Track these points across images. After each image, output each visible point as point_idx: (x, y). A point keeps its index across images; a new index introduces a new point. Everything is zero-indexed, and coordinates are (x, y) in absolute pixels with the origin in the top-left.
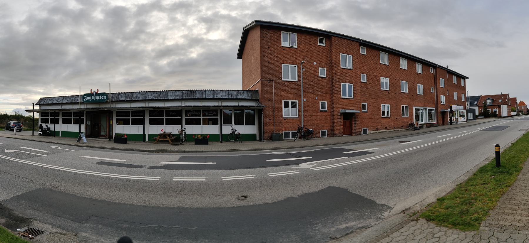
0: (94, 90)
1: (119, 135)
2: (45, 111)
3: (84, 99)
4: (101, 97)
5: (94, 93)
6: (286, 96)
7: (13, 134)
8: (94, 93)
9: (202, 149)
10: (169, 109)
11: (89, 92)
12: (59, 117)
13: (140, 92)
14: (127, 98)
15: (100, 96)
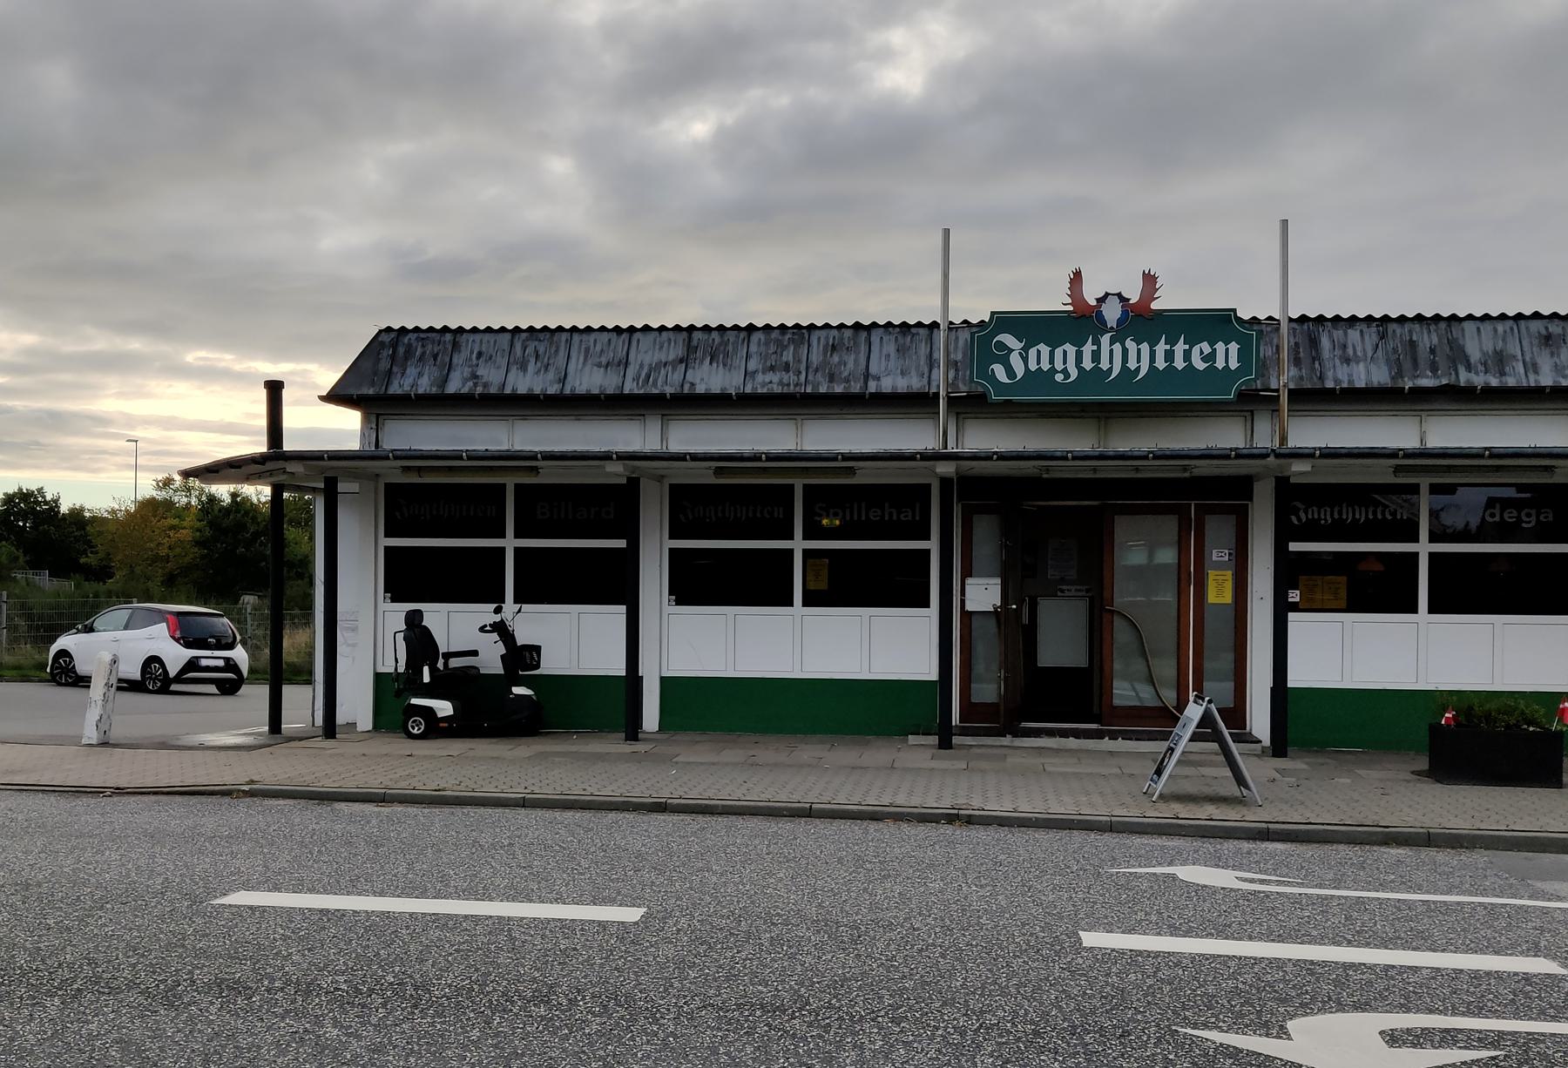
1: (1492, 706)
4: (1180, 347)
5: (1112, 313)
7: (75, 741)
8: (1112, 313)
10: (851, 471)
11: (1056, 300)
14: (1407, 365)
15: (1172, 342)
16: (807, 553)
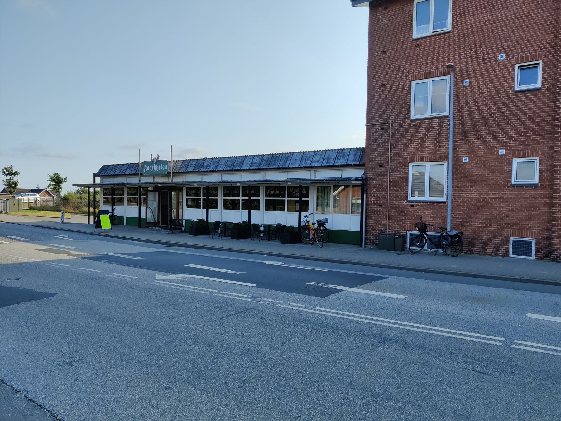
0: (155, 156)
4: (161, 166)
5: (155, 161)
6: (417, 155)
8: (155, 161)
11: (149, 160)
12: (259, 197)
16: (242, 200)
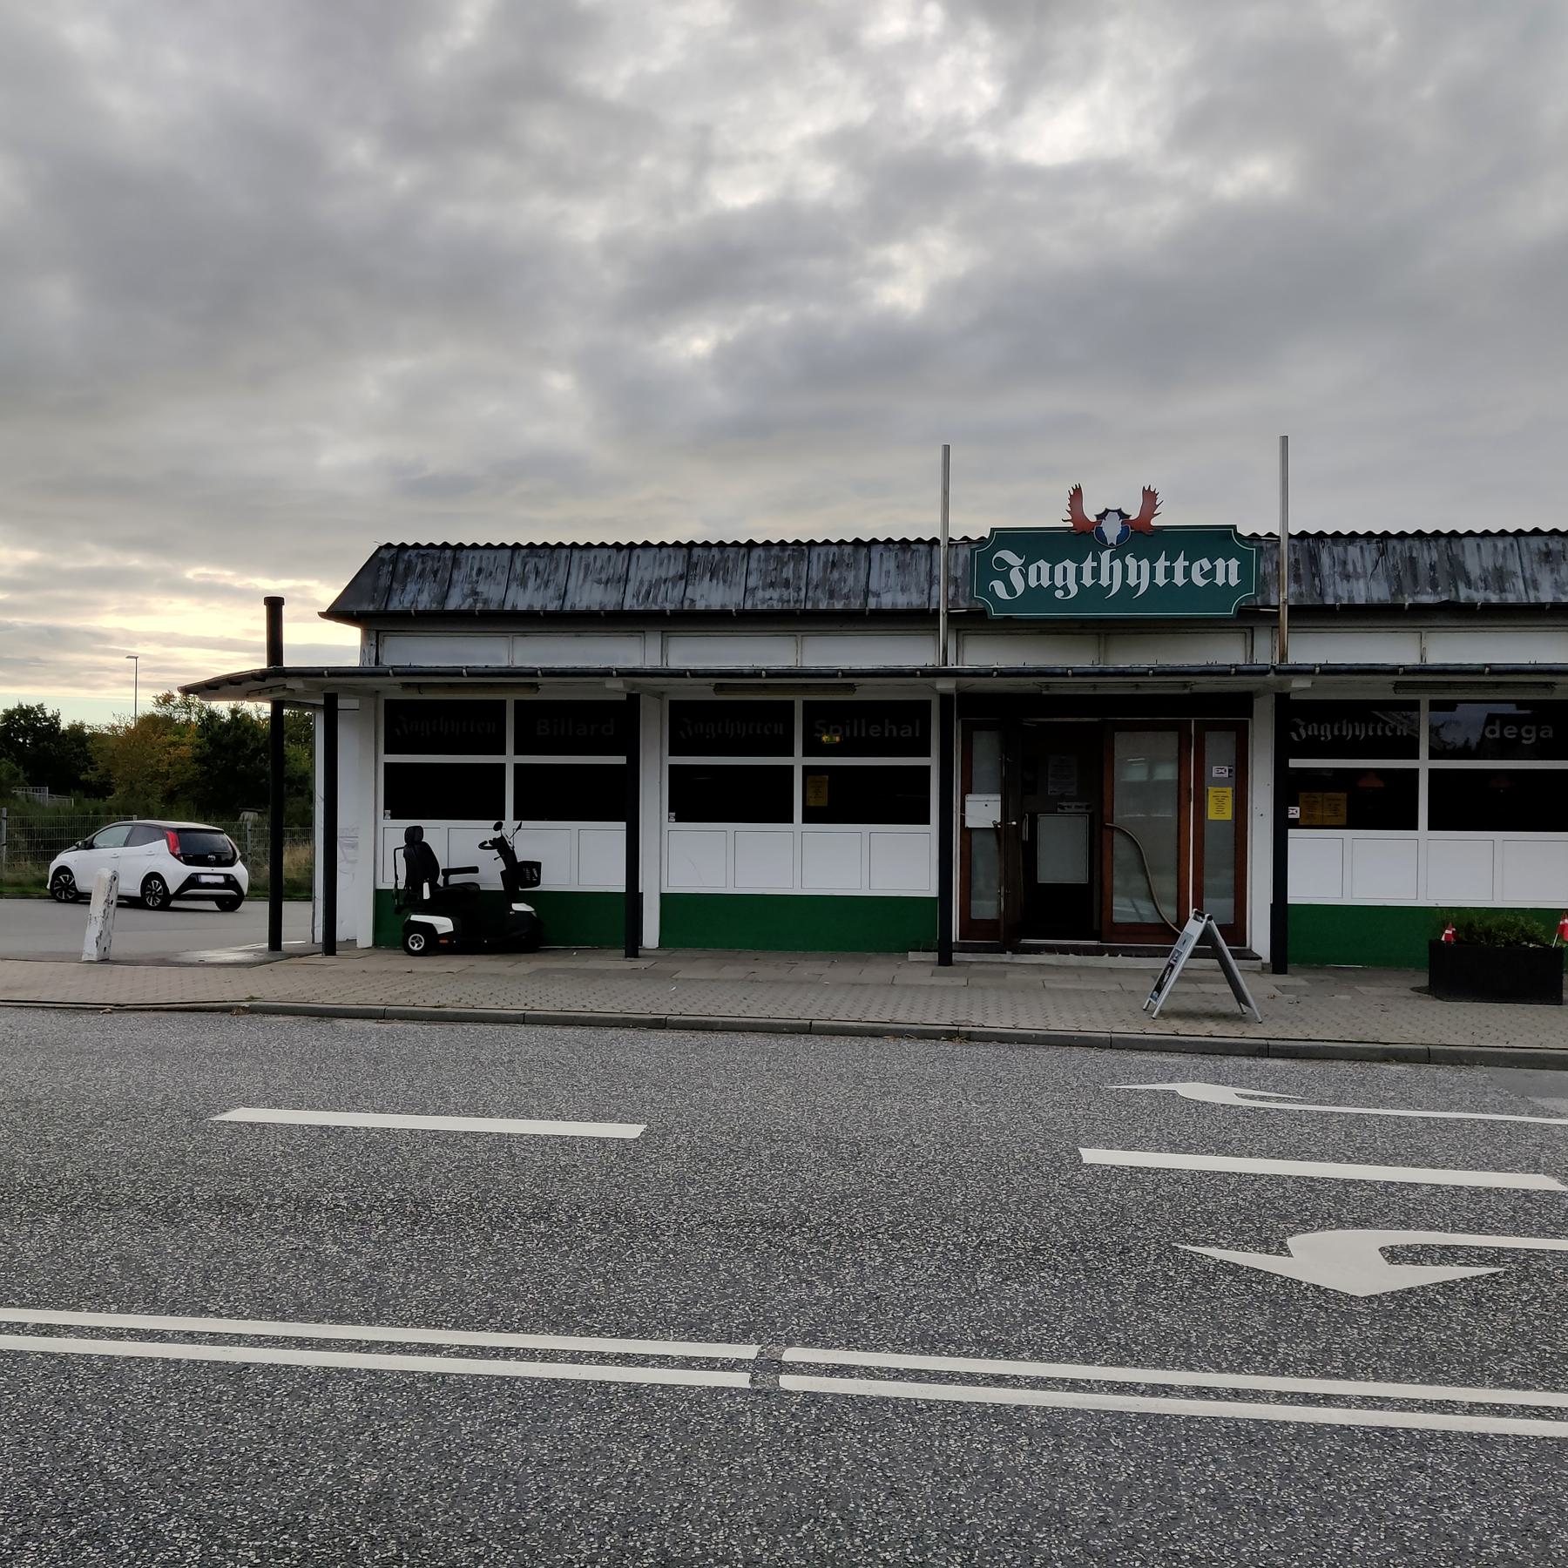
1: (1491, 923)
2: (535, 686)
3: (999, 588)
4: (1180, 564)
5: (1112, 529)
7: (75, 957)
8: (1112, 529)
9: (901, 1016)
11: (1056, 517)
13: (1519, 533)
14: (1407, 582)
